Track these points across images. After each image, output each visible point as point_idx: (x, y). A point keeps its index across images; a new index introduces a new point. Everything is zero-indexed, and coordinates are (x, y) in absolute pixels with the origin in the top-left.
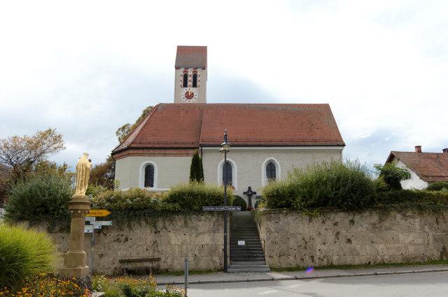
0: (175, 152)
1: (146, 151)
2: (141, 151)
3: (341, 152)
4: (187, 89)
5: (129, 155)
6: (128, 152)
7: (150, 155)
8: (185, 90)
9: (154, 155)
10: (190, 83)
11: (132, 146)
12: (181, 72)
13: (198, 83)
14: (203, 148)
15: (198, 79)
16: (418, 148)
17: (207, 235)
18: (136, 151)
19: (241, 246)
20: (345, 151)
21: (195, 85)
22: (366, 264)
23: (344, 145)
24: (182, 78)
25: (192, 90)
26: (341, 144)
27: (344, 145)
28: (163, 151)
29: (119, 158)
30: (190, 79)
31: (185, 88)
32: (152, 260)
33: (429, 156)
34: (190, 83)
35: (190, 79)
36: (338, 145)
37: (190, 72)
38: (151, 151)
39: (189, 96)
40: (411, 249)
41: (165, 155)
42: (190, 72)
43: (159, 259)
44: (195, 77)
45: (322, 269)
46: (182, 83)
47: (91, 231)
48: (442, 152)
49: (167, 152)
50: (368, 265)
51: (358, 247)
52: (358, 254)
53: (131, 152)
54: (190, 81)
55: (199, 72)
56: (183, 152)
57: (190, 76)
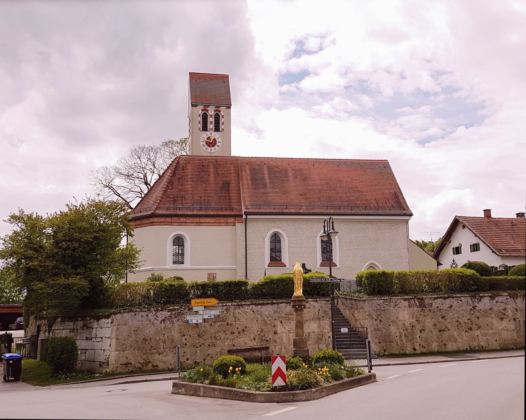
0: (212, 220)
1: (175, 219)
2: (168, 220)
3: (407, 221)
4: (208, 133)
5: (152, 224)
6: (152, 220)
7: (180, 224)
8: (205, 135)
9: (185, 224)
10: (211, 126)
11: (158, 212)
12: (199, 110)
13: (222, 127)
14: (249, 217)
15: (222, 120)
16: (487, 212)
17: (312, 323)
18: (162, 220)
19: (344, 334)
20: (412, 221)
21: (217, 129)
22: (464, 351)
23: (411, 215)
24: (200, 119)
25: (215, 135)
26: (407, 213)
27: (411, 215)
28: (197, 220)
29: (137, 227)
30: (211, 120)
31: (205, 133)
32: (260, 349)
33: (498, 222)
34: (211, 126)
35: (211, 120)
36: (405, 215)
37: (211, 111)
38: (182, 219)
39: (211, 143)
40: (504, 334)
41: (199, 224)
42: (211, 111)
43: (267, 348)
44: (217, 118)
45: (414, 357)
46: (200, 126)
47: (200, 321)
48: (515, 217)
49: (202, 220)
50: (466, 351)
51: (455, 333)
52: (455, 341)
53: (156, 220)
54: (211, 123)
55: (223, 111)
56: (222, 220)
57: (211, 116)
